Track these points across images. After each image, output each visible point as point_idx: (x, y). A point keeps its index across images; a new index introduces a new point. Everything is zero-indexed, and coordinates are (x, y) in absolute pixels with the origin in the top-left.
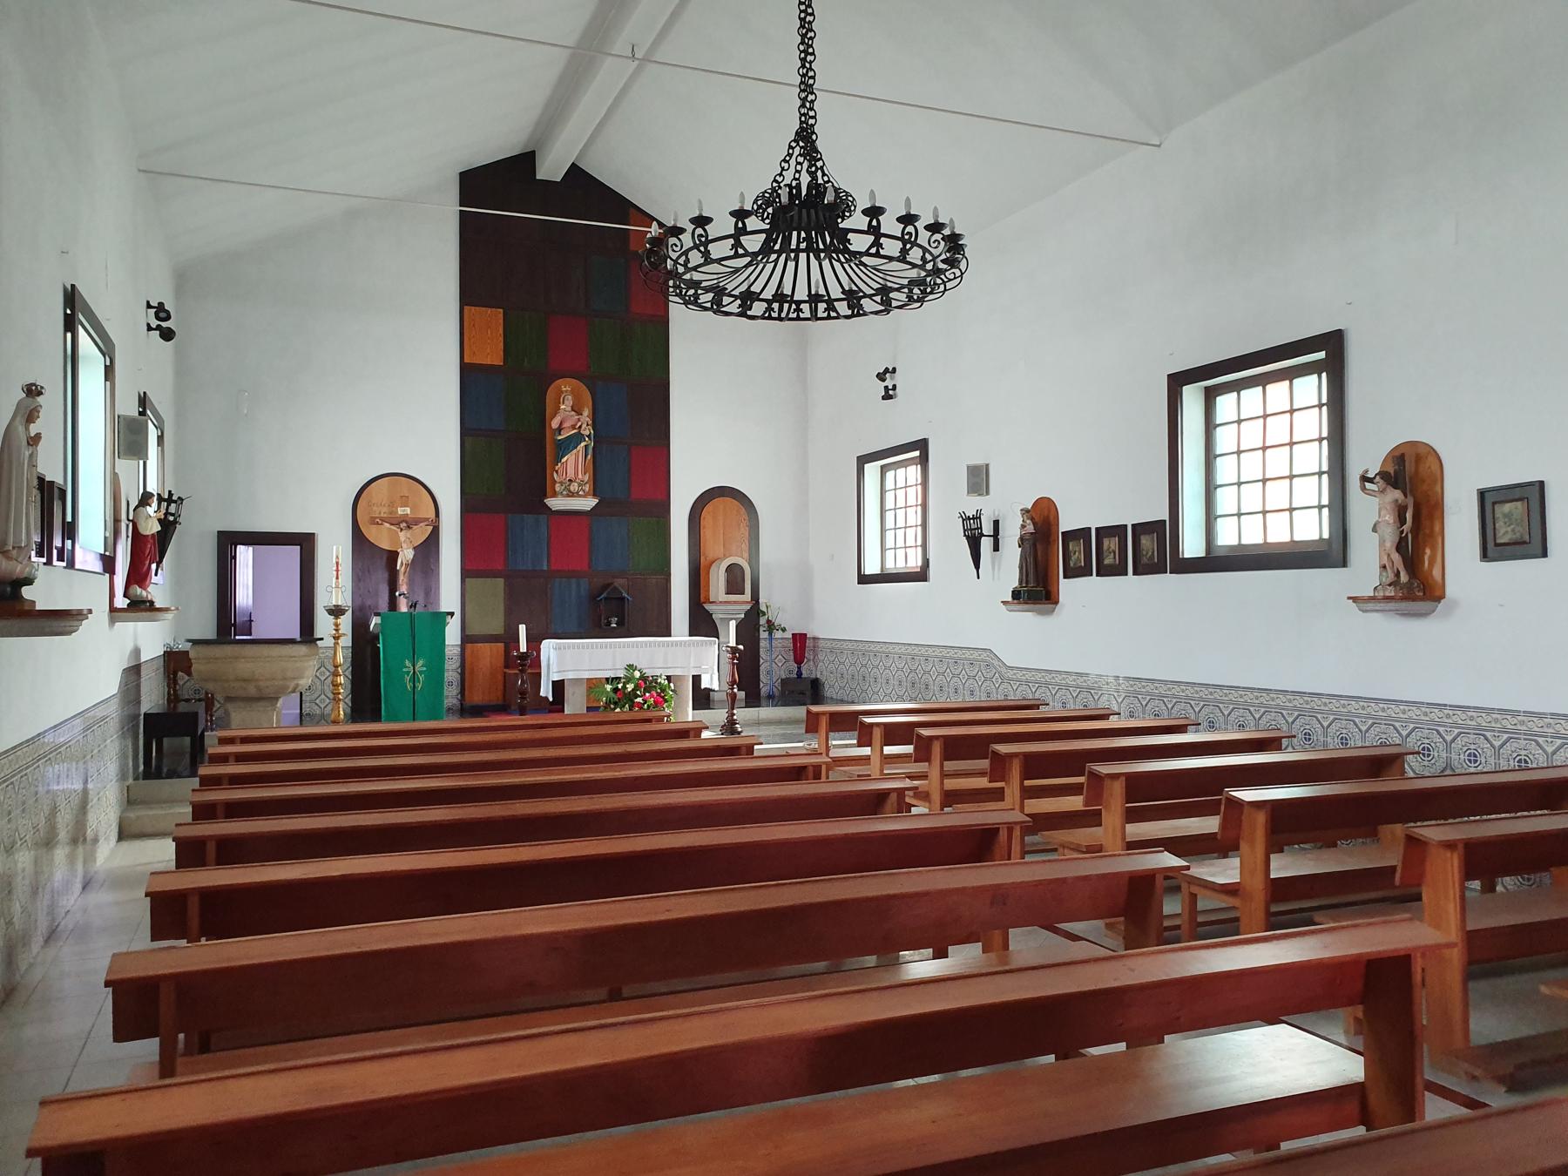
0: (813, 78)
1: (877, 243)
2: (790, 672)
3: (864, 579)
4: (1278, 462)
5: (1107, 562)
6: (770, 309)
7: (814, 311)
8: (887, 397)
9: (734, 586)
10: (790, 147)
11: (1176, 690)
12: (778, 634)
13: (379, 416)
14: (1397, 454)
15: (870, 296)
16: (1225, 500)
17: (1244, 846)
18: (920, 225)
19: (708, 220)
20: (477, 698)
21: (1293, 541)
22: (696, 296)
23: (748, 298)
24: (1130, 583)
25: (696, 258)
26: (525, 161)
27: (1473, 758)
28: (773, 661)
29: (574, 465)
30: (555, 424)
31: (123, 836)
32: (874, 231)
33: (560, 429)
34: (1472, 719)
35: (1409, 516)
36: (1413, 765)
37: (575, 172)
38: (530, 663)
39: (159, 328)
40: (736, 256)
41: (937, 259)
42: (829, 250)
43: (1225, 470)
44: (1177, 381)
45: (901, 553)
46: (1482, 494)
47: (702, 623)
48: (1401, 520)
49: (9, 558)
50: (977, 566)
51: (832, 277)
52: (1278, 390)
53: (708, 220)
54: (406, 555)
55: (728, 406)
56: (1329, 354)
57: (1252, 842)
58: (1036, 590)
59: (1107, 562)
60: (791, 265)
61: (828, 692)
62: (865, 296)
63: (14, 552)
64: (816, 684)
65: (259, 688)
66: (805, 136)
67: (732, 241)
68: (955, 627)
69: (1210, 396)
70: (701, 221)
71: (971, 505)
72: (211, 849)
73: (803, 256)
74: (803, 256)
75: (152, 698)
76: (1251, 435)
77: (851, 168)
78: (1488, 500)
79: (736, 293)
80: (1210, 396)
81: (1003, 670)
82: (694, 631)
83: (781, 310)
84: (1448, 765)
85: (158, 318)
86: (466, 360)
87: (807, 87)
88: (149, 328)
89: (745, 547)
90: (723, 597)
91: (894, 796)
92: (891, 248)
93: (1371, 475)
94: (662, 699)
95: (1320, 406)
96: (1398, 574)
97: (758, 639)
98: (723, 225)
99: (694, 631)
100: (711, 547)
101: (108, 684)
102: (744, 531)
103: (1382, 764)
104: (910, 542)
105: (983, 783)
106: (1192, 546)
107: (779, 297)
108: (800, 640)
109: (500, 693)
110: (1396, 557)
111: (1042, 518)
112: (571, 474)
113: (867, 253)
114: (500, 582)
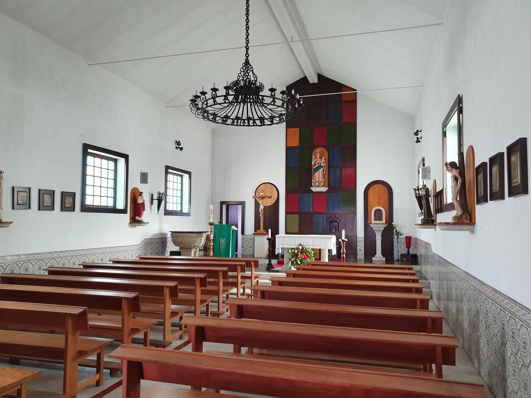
1: (274, 101)
6: (233, 122)
7: (249, 123)
15: (267, 119)
22: (208, 116)
23: (272, 118)
25: (211, 102)
32: (273, 96)
33: (315, 165)
40: (225, 103)
42: (256, 102)
50: (158, 210)
51: (257, 111)
53: (217, 90)
62: (266, 119)
73: (242, 104)
79: (222, 116)
83: (237, 122)
97: (393, 238)
98: (222, 92)
107: (237, 118)
113: (270, 104)
114: (297, 216)
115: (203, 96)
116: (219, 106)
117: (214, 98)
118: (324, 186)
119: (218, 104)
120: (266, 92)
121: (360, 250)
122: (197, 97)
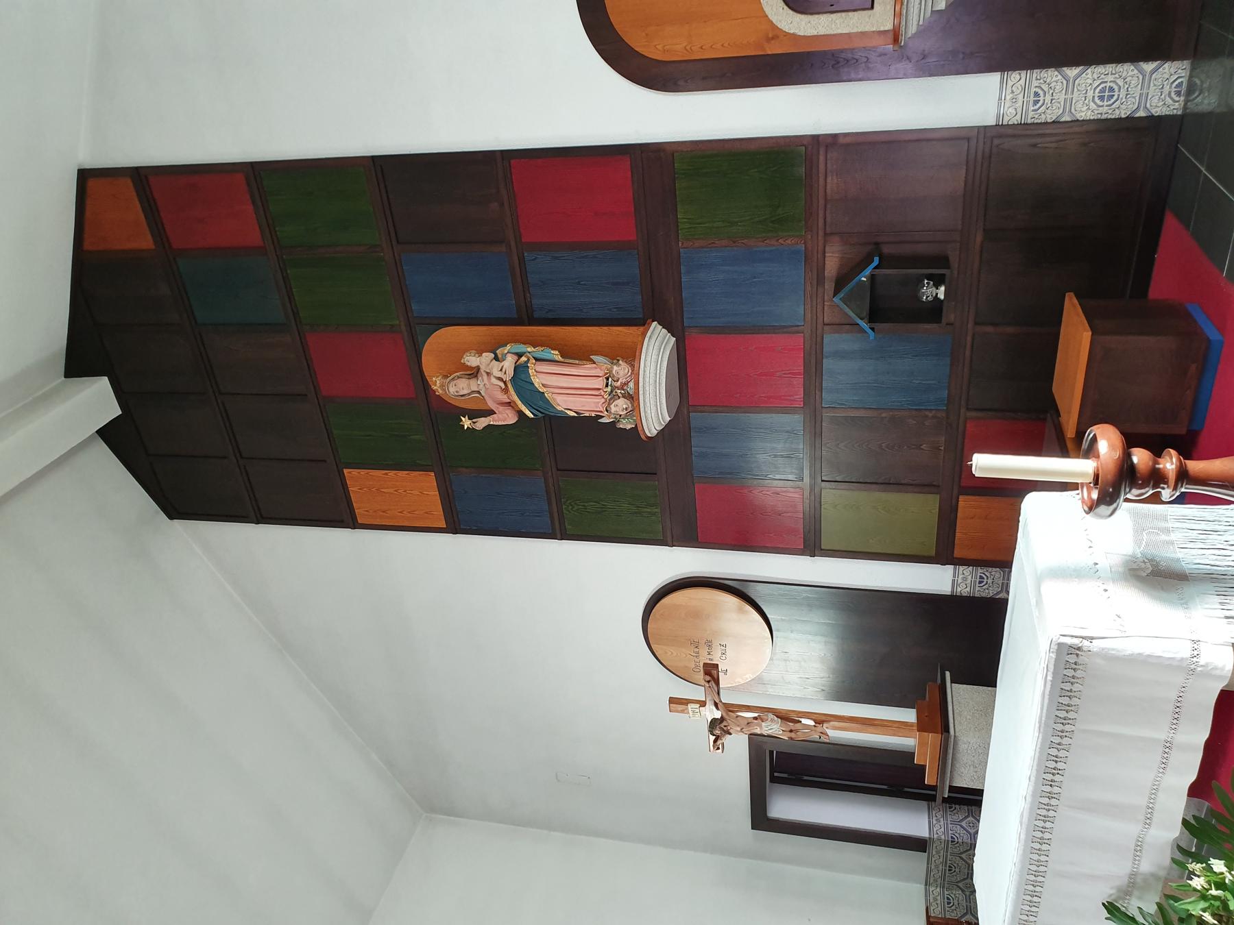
118: (631, 355)
121: (1107, 94)
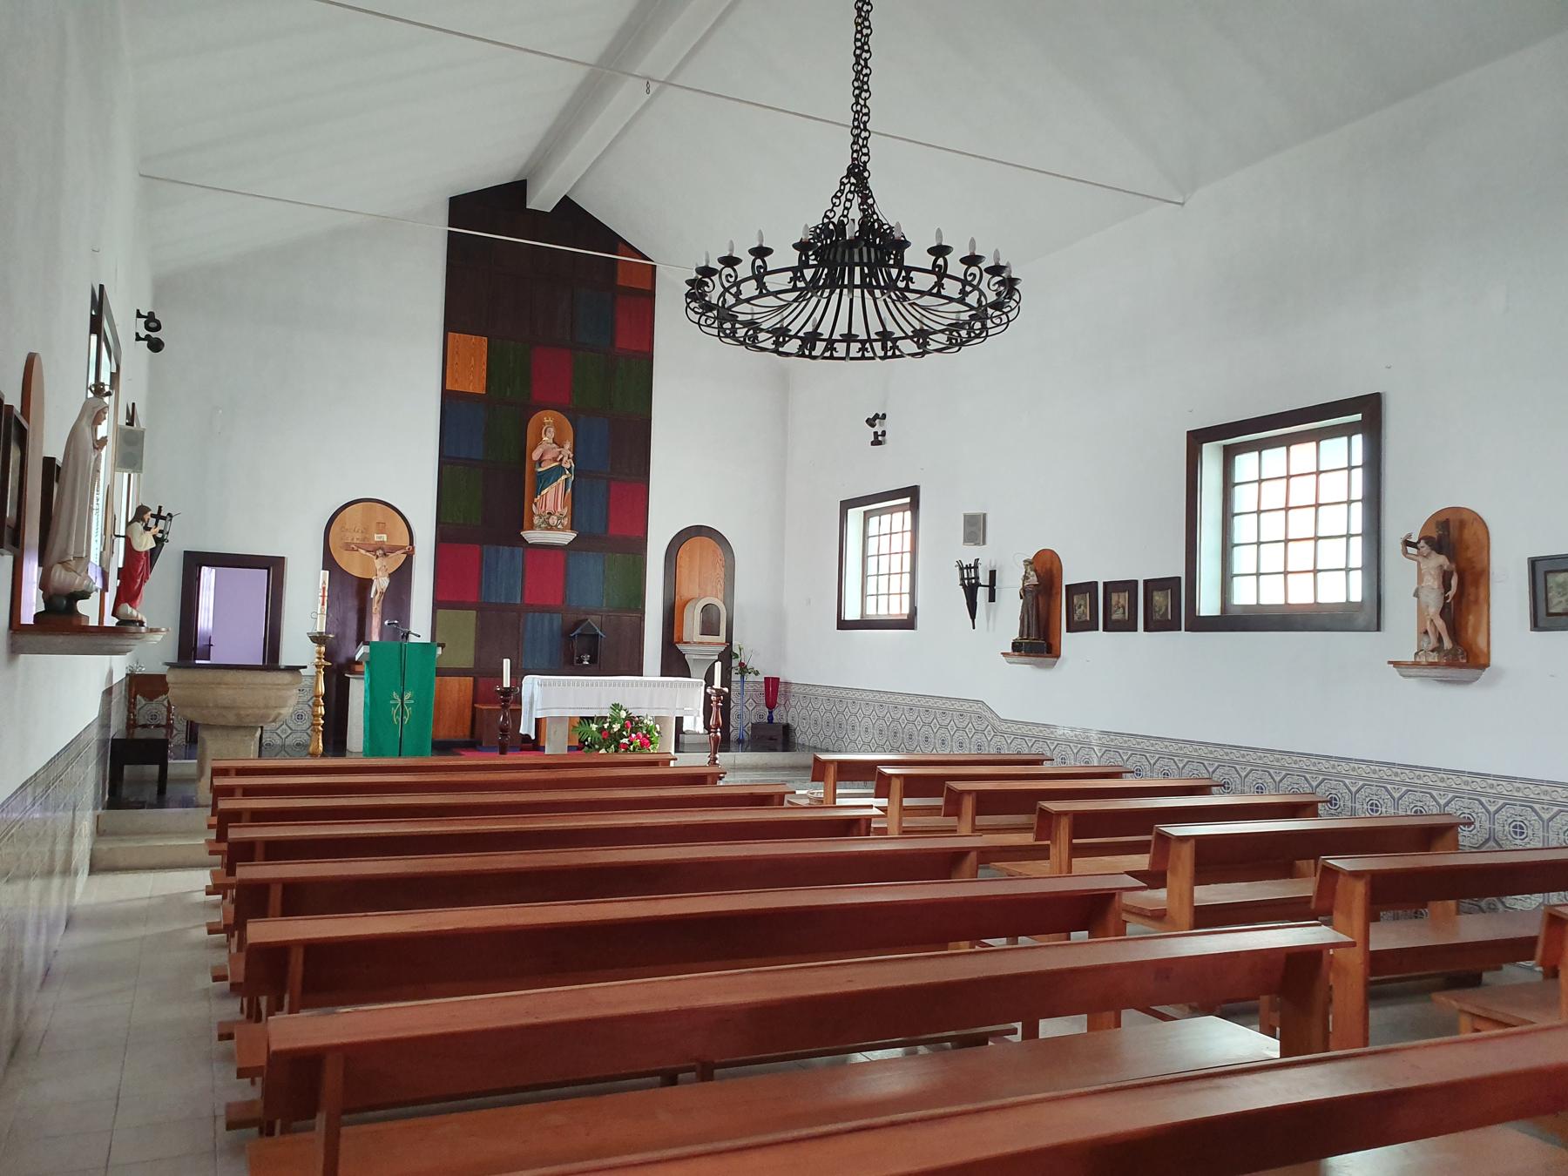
0: (867, 114)
2: (761, 716)
3: (843, 625)
4: (1302, 523)
5: (1115, 617)
8: (876, 442)
9: (709, 627)
10: (842, 183)
11: (1188, 750)
12: (750, 678)
13: (350, 442)
14: (1465, 516)
16: (1243, 560)
17: (1338, 917)
18: (983, 266)
19: (768, 251)
20: (443, 735)
21: (1316, 603)
22: (734, 330)
24: (1140, 638)
25: (749, 289)
26: (516, 190)
27: (1519, 830)
28: (744, 705)
29: (553, 498)
30: (536, 456)
31: (93, 870)
32: (940, 273)
33: (540, 462)
34: (1518, 790)
35: (1454, 582)
36: (1465, 836)
37: (566, 204)
38: (512, 699)
39: (147, 338)
40: (795, 289)
41: (988, 298)
43: (1243, 529)
44: (1197, 439)
45: (883, 599)
46: (1533, 563)
47: (674, 664)
48: (1446, 586)
49: (67, 569)
50: (973, 616)
52: (1303, 454)
53: (768, 251)
54: (381, 583)
55: (717, 441)
56: (1366, 415)
57: (1349, 915)
58: (1037, 642)
59: (1115, 617)
60: (835, 297)
61: (800, 738)
63: (73, 563)
64: (787, 729)
65: (238, 715)
66: (857, 174)
67: (790, 274)
68: (969, 681)
69: (1229, 455)
70: (761, 252)
71: (969, 555)
72: (276, 896)
74: (857, 292)
75: (117, 728)
76: (1273, 495)
77: (912, 208)
78: (1541, 570)
80: (1229, 455)
81: (997, 723)
82: (666, 671)
84: (1492, 837)
85: (147, 328)
86: (448, 387)
87: (860, 125)
88: (138, 338)
89: (720, 587)
90: (697, 637)
91: (973, 855)
92: (952, 288)
93: (1414, 539)
94: (647, 741)
95: (1350, 468)
96: (1440, 639)
98: (784, 256)
99: (666, 671)
100: (686, 589)
101: (90, 711)
102: (721, 572)
103: (1431, 835)
104: (895, 589)
105: (1028, 839)
106: (1208, 605)
108: (772, 685)
109: (468, 733)
110: (1440, 623)
111: (1045, 570)
112: (550, 507)
113: (929, 293)
115: (728, 271)
116: (771, 301)
117: (759, 276)
119: (769, 293)
120: (916, 256)
122: (707, 272)
